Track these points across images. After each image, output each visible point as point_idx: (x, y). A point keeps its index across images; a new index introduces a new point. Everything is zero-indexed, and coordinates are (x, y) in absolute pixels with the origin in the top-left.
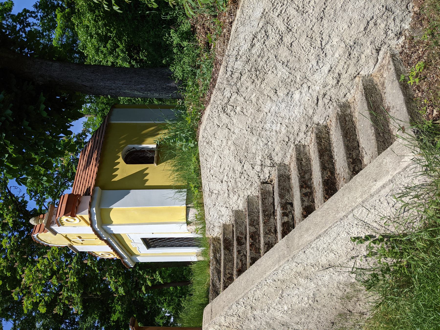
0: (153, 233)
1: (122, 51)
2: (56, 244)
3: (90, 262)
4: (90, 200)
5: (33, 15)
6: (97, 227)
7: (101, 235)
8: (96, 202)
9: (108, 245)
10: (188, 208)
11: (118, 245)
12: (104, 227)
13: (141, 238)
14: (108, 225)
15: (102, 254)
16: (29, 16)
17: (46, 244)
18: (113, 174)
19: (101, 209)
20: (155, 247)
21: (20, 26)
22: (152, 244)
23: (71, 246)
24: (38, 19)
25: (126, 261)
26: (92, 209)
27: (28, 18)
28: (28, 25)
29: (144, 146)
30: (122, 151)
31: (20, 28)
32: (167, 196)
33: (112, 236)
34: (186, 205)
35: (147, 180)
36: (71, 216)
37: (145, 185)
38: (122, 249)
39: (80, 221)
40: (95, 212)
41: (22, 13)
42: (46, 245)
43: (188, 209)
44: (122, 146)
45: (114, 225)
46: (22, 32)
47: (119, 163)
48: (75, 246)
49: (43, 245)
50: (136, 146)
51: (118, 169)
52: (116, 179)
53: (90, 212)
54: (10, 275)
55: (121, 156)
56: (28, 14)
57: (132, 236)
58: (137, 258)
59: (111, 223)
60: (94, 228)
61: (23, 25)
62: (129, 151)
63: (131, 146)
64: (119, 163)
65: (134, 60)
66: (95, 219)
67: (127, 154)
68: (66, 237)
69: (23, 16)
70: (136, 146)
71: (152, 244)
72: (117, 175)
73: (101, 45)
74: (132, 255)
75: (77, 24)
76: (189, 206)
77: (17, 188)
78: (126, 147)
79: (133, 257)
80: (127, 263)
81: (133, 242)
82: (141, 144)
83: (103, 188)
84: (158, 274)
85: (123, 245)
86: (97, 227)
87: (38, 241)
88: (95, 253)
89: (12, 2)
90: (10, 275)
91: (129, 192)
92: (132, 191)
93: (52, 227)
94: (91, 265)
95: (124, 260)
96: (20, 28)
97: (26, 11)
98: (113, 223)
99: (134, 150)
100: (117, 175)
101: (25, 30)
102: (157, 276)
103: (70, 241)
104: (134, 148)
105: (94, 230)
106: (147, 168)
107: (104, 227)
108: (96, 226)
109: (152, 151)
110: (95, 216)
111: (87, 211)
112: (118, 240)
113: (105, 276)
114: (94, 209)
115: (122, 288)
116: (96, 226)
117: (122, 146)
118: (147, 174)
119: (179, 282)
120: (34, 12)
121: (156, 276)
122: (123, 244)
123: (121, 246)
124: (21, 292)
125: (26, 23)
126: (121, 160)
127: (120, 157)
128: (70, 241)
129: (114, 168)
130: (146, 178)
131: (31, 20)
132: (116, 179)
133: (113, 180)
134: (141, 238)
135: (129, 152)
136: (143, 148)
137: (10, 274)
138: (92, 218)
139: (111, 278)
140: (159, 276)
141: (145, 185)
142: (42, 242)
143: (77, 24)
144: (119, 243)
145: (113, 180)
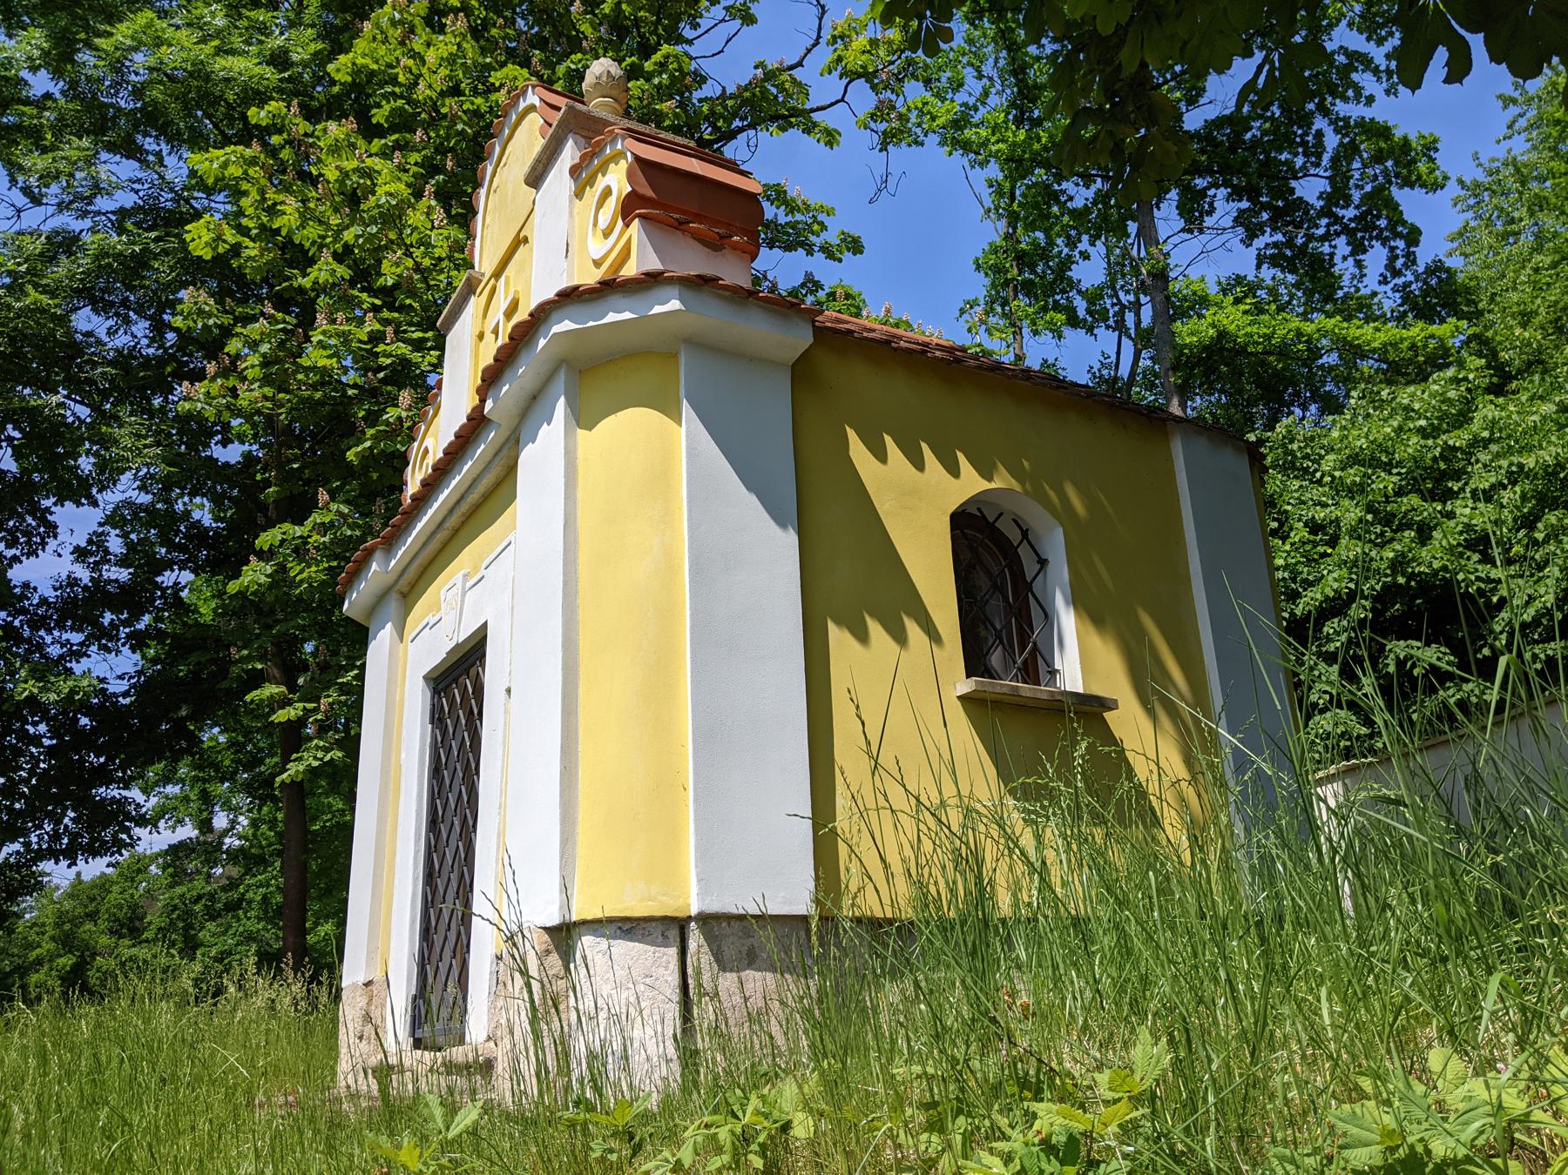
0: (509, 691)
1: (1398, 564)
2: (488, 220)
3: (400, 418)
4: (728, 280)
5: (1399, 263)
6: (556, 329)
7: (508, 375)
8: (716, 318)
9: (457, 436)
10: (674, 933)
11: (458, 502)
12: (560, 381)
13: (485, 625)
14: (569, 403)
15: (426, 451)
16: (1392, 249)
17: (490, 170)
18: (888, 439)
19: (674, 356)
20: (437, 718)
21: (1350, 220)
22: (452, 703)
23: (471, 288)
24: (1385, 278)
25: (374, 566)
26: (675, 290)
27: (1384, 244)
28: (1358, 248)
29: (1068, 620)
30: (1026, 493)
31: (1343, 217)
32: (899, 714)
33: (505, 451)
34: (705, 919)
35: (863, 637)
36: (629, 195)
37: (832, 627)
38: (433, 534)
39: (598, 264)
40: (657, 309)
41: (1404, 223)
42: (485, 169)
43: (672, 928)
44: (1052, 494)
45: (569, 435)
46: (1328, 226)
47: (954, 471)
48: (474, 305)
49: (483, 160)
50: (1060, 571)
51: (919, 466)
52: (858, 451)
53: (651, 280)
54: (374, 121)
55: (992, 486)
56: (1401, 244)
57: (501, 572)
58: (389, 625)
59: (583, 418)
60: (555, 316)
61: (1355, 230)
62: (1025, 534)
63: (1055, 545)
64: (954, 471)
65: (1373, 610)
66: (612, 317)
67: (1006, 527)
68: (519, 241)
69: (1392, 226)
70: (1060, 571)
71: (452, 703)
72: (881, 456)
73: (1399, 474)
74: (404, 596)
75: (1466, 379)
76: (695, 940)
77: (753, 149)
78: (1048, 517)
79: (393, 605)
80: (363, 575)
81: (469, 584)
82: (1078, 600)
83: (802, 373)
84: (328, 758)
85: (456, 531)
86: (556, 329)
87: (502, 130)
88: (435, 415)
89: (1442, 188)
90: (374, 121)
91: (782, 524)
92: (791, 539)
93: (570, 144)
94: (387, 423)
95: (378, 555)
96: (1343, 217)
97: (1413, 236)
98: (581, 433)
99: (1030, 567)
100: (881, 456)
101: (1338, 234)
102: (320, 754)
103: (497, 275)
104: (1043, 563)
105: (542, 314)
106: (934, 636)
107: (560, 381)
108: (567, 325)
109: (1036, 665)
110: (627, 315)
111: (655, 264)
112: (486, 497)
113: (333, 499)
114: (675, 305)
115: (263, 579)
116: (567, 325)
117: (1052, 494)
118: (900, 638)
119: (304, 867)
120: (1414, 262)
121: (318, 748)
122: (462, 534)
123: (453, 521)
124: (289, 142)
125: (1363, 238)
126: (970, 484)
127: (990, 480)
128: (497, 275)
129: (924, 446)
130: (875, 628)
131: (1376, 257)
132: (858, 451)
133: (852, 435)
134: (485, 625)
135: (1014, 535)
136: (1048, 616)
137: (382, 121)
138: (616, 299)
139: (323, 528)
140: (316, 764)
141: (831, 626)
142: (497, 149)
143: (1466, 379)
144: (464, 507)
145: (852, 435)
